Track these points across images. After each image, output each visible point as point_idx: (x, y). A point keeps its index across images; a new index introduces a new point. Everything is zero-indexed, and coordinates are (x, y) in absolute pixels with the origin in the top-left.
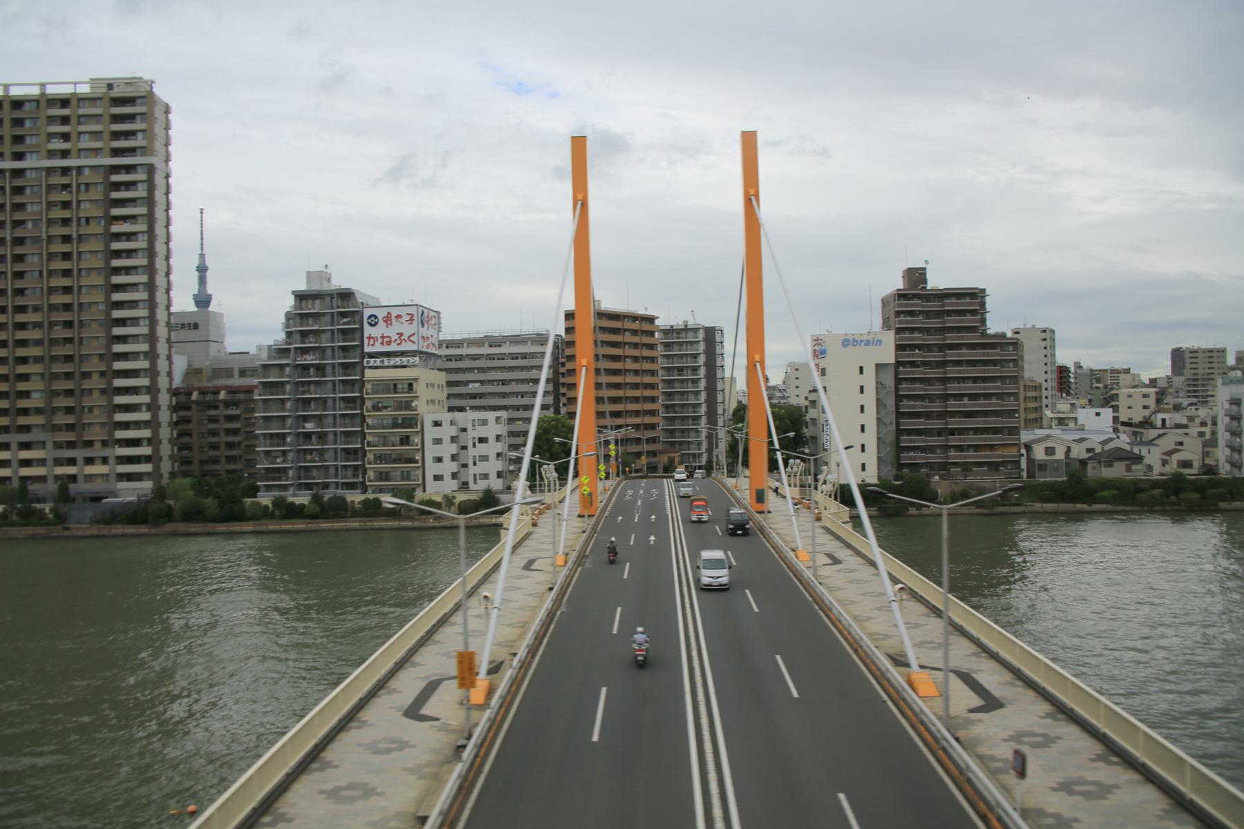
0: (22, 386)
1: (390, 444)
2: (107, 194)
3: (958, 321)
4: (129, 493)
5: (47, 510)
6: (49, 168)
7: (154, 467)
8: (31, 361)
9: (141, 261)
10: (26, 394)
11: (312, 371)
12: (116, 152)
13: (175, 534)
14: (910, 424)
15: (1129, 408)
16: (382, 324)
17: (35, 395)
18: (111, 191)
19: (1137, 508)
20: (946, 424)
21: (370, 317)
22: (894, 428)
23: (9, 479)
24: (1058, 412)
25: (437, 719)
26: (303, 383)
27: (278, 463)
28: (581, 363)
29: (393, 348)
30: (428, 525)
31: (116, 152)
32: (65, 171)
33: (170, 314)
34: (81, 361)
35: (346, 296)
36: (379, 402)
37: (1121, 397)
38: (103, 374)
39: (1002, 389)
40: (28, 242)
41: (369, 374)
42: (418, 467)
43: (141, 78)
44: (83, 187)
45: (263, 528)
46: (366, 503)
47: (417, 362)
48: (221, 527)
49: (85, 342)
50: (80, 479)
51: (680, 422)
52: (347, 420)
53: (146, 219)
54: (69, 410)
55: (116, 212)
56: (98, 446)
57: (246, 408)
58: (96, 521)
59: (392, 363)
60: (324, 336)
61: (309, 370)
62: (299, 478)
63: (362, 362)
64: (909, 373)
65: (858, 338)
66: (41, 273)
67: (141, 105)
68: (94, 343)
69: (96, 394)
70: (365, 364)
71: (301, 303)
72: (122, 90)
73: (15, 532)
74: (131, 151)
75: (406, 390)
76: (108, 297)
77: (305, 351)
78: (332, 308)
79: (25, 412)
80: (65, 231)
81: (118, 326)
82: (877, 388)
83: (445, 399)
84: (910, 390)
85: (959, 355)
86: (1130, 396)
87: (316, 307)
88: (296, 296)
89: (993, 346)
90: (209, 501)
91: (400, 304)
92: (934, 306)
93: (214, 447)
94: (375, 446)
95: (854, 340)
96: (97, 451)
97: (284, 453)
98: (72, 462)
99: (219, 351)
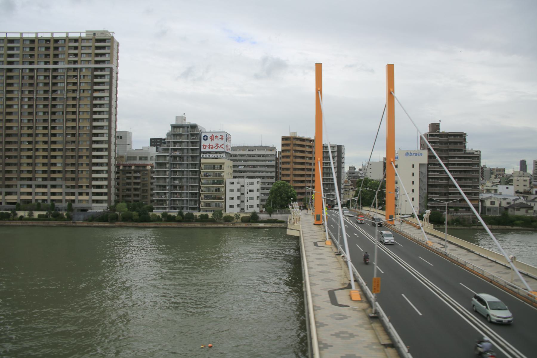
0: (53, 161)
1: (212, 191)
2: (92, 80)
3: (454, 147)
4: (99, 208)
5: (65, 214)
6: (68, 68)
7: (108, 198)
8: (57, 150)
9: (106, 109)
10: (55, 164)
11: (178, 159)
12: (97, 62)
13: (121, 227)
14: (433, 190)
15: (517, 185)
16: (209, 140)
17: (58, 165)
18: (94, 79)
19: (533, 229)
20: (448, 190)
21: (204, 136)
22: (427, 191)
23: (46, 200)
24: (487, 187)
25: (349, 306)
26: (174, 163)
27: (162, 198)
28: (317, 160)
29: (214, 150)
30: (230, 226)
31: (97, 62)
32: (75, 69)
33: (116, 132)
34: (78, 151)
35: (194, 127)
36: (207, 173)
37: (514, 181)
38: (87, 157)
39: (473, 176)
40: (58, 99)
41: (203, 161)
42: (223, 202)
43: (107, 31)
44: (82, 77)
45: (158, 225)
46: (201, 216)
47: (224, 156)
48: (140, 225)
49: (80, 143)
50: (76, 201)
51: (326, 186)
52: (192, 180)
53: (108, 91)
54: (73, 172)
55: (96, 87)
56: (84, 187)
57: (143, 174)
58: (86, 220)
59: (213, 156)
60: (183, 144)
61: (176, 158)
62: (171, 204)
63: (201, 155)
64: (433, 168)
65: (412, 153)
66: (63, 113)
67: (108, 42)
68: (85, 143)
69: (85, 165)
70: (201, 157)
71: (174, 129)
72: (100, 36)
73: (52, 223)
74: (103, 62)
75: (219, 168)
76: (91, 124)
77: (175, 150)
78: (188, 132)
79: (54, 172)
80: (74, 95)
81: (94, 136)
82: (419, 174)
83: (232, 173)
84: (433, 175)
85: (454, 161)
86: (518, 181)
87: (180, 131)
88: (172, 126)
89: (469, 158)
90: (134, 213)
91: (209, 131)
92: (444, 140)
93: (129, 190)
94: (205, 192)
95: (410, 153)
96: (84, 190)
97: (165, 193)
98: (73, 194)
99: (130, 149)
